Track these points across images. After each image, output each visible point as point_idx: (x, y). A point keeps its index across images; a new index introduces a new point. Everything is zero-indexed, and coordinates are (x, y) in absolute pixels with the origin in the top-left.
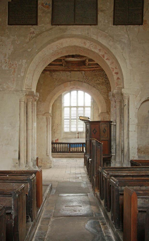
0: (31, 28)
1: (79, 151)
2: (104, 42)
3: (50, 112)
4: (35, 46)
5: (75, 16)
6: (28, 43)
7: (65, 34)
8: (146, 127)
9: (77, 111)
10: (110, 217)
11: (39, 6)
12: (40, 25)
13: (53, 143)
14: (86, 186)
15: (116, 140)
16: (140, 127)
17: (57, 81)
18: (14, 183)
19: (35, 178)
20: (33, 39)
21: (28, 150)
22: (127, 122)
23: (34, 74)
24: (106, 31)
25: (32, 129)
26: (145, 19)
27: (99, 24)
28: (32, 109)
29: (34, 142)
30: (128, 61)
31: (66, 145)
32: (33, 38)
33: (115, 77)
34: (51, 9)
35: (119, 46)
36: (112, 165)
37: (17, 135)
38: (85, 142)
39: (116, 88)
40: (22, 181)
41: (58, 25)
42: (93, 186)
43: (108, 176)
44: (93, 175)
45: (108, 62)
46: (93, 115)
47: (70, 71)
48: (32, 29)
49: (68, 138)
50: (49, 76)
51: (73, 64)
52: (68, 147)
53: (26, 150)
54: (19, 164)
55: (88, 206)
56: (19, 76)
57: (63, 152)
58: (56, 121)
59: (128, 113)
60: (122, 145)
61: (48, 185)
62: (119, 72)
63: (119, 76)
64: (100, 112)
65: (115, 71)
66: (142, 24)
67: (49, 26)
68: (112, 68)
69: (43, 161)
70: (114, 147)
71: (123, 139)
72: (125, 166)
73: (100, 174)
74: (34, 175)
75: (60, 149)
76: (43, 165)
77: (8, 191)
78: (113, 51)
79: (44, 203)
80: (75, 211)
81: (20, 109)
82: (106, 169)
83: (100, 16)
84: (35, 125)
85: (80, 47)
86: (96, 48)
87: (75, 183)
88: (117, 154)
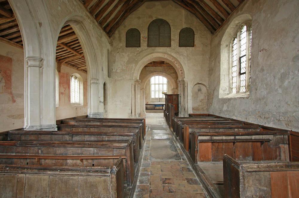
2: (174, 55)
6: (135, 56)
10: (178, 139)
11: (141, 38)
12: (142, 47)
15: (181, 104)
30: (186, 65)
33: (180, 72)
34: (147, 39)
35: (182, 57)
36: (179, 116)
37: (130, 101)
38: (165, 104)
40: (139, 123)
42: (169, 127)
43: (177, 121)
44: (169, 121)
45: (177, 65)
47: (156, 66)
48: (138, 49)
52: (154, 107)
55: (168, 135)
62: (182, 70)
63: (182, 72)
64: (172, 88)
66: (194, 47)
67: (146, 48)
72: (186, 116)
73: (173, 120)
74: (143, 120)
81: (132, 88)
83: (172, 43)
84: (139, 96)
85: (162, 58)
87: (160, 125)
88: (182, 111)
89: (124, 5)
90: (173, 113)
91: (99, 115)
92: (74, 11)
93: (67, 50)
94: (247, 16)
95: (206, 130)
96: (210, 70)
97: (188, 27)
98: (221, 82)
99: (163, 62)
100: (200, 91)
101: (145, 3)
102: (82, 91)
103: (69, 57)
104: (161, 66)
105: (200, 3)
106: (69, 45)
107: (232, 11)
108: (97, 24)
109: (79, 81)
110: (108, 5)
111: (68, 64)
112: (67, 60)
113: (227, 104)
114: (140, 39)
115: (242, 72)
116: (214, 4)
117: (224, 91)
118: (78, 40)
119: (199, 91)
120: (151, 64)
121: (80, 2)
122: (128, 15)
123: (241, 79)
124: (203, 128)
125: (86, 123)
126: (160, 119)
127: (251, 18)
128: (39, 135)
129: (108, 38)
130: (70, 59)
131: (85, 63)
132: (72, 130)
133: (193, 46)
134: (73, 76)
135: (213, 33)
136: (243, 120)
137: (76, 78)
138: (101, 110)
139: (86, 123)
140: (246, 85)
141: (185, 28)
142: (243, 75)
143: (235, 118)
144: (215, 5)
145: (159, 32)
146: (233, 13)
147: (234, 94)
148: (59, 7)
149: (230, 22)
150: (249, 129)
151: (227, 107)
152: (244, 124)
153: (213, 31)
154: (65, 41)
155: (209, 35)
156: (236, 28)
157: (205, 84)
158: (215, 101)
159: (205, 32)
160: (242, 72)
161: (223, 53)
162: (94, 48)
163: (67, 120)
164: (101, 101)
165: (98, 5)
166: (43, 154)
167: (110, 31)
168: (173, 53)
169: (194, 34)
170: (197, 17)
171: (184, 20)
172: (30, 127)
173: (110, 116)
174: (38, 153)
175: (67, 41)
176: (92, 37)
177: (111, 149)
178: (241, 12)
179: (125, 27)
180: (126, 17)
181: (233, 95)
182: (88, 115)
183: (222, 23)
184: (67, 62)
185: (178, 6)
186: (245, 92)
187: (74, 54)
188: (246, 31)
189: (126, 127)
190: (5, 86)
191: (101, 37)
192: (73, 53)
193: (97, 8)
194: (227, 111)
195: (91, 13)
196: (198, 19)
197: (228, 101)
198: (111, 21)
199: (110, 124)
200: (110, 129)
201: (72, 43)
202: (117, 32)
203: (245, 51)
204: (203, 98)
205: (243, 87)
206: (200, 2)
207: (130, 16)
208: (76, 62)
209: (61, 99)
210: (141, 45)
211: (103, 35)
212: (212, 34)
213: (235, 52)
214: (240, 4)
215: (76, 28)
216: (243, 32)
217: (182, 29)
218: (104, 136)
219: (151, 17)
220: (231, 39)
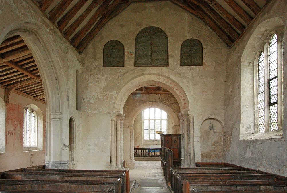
0: (119, 69)
1: (157, 155)
2: (174, 78)
3: (133, 125)
4: (122, 81)
5: (152, 60)
6: (117, 79)
7: (144, 72)
8: (208, 138)
9: (155, 123)
11: (126, 54)
12: (126, 67)
13: (135, 149)
14: (162, 182)
15: (184, 148)
16: (202, 138)
17: (138, 102)
18: (112, 178)
19: (126, 175)
20: (121, 77)
22: (192, 135)
24: (175, 70)
25: (120, 140)
27: (170, 65)
28: (120, 126)
29: (122, 149)
31: (146, 150)
32: (121, 76)
33: (183, 102)
34: (134, 55)
35: (185, 81)
36: (182, 167)
39: (184, 111)
40: (118, 177)
41: (140, 67)
42: (167, 182)
43: (176, 174)
45: (177, 92)
46: (169, 126)
47: (149, 94)
48: (120, 69)
49: (148, 145)
52: (148, 152)
53: (116, 156)
54: (111, 166)
56: (111, 102)
57: (143, 156)
58: (138, 131)
59: (193, 128)
60: (189, 152)
61: (133, 181)
63: (185, 101)
64: (173, 125)
65: (183, 98)
66: (202, 65)
67: (133, 67)
68: (180, 96)
69: (128, 163)
71: (189, 147)
72: (191, 167)
74: (124, 173)
75: (141, 153)
76: (127, 166)
77: (111, 182)
78: (181, 85)
82: (175, 169)
83: (171, 60)
84: (122, 137)
85: (156, 81)
86: (167, 82)
89: (99, 8)
90: (171, 160)
91: (61, 164)
92: (23, 16)
94: (275, 21)
95: (216, 187)
96: (226, 98)
97: (194, 38)
98: (242, 116)
99: (159, 88)
100: (212, 130)
101: (131, 5)
102: (41, 130)
103: (21, 81)
104: (156, 94)
105: (210, 4)
106: (20, 64)
107: (256, 15)
108: (59, 34)
109: (37, 115)
110: (77, 8)
111: (21, 91)
112: (19, 85)
113: (251, 148)
115: (272, 102)
117: (247, 129)
118: (32, 57)
119: (211, 129)
120: (142, 90)
121: (33, 4)
122: (107, 22)
123: (271, 112)
124: (211, 185)
125: (40, 178)
126: (156, 171)
127: (282, 23)
129: (77, 54)
130: (24, 84)
131: (43, 91)
132: (16, 187)
133: (201, 65)
134: (27, 108)
135: (230, 46)
136: (275, 172)
137: (32, 111)
138: (66, 158)
139: (40, 178)
140: (279, 120)
141: (189, 39)
142: (273, 106)
143: (262, 169)
144: (230, 6)
145: (151, 45)
146: (258, 16)
147: (261, 134)
149: (252, 30)
150: (283, 186)
152: (277, 178)
154: (14, 58)
155: (224, 49)
156: (262, 38)
157: (219, 119)
158: (233, 143)
159: (218, 45)
160: (272, 102)
161: (245, 74)
162: (55, 69)
163: (11, 173)
164: (66, 144)
165: (61, 8)
167: (80, 44)
168: (171, 74)
169: (202, 48)
170: (206, 23)
171: (187, 28)
173: (79, 167)
175: (17, 59)
176: (52, 54)
178: (268, 15)
179: (102, 38)
180: (104, 24)
181: (261, 134)
182: (46, 165)
183: (242, 31)
184: (20, 89)
186: (278, 131)
187: (28, 77)
188: (277, 42)
189: (97, 183)
191: (66, 53)
192: (27, 76)
194: (251, 158)
195: (52, 18)
196: (208, 27)
197: (253, 144)
198: (81, 30)
199: (75, 178)
200: (73, 185)
202: (90, 46)
203: (276, 70)
204: (217, 140)
205: (274, 123)
206: (210, 3)
207: (109, 23)
208: (33, 89)
209: (8, 142)
210: (125, 63)
213: (262, 73)
214: (266, 4)
215: (28, 40)
216: (273, 43)
217: (185, 41)
219: (139, 24)
220: (256, 55)
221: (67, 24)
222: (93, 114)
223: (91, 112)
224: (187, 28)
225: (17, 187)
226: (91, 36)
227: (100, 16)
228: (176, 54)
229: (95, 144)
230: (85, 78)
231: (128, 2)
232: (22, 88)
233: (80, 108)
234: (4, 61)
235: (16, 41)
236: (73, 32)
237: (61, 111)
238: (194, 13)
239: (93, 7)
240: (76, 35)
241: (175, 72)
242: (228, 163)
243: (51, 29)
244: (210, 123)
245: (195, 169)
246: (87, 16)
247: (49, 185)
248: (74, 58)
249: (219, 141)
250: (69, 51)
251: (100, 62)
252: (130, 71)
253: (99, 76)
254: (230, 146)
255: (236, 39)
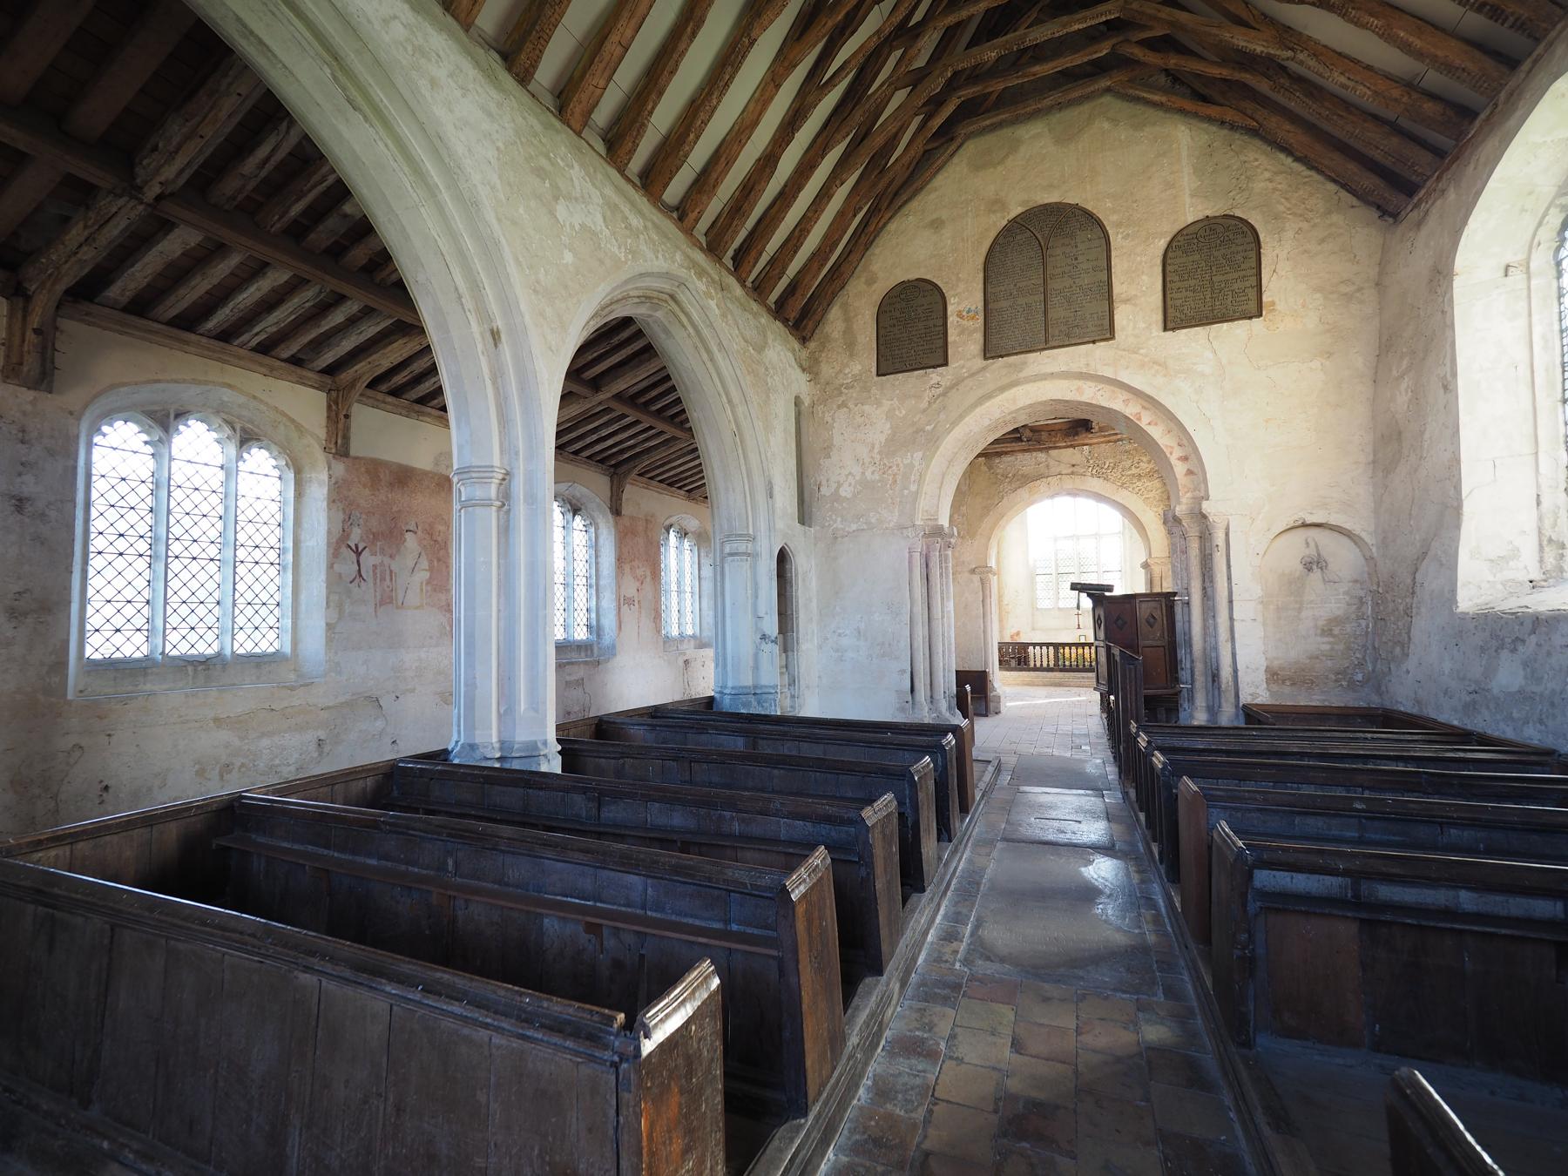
4: (942, 416)
6: (924, 411)
7: (1022, 375)
11: (952, 319)
12: (954, 364)
16: (1271, 607)
21: (934, 670)
23: (942, 483)
25: (943, 617)
26: (1270, 299)
28: (941, 568)
29: (950, 650)
41: (1002, 357)
48: (935, 376)
50: (984, 468)
51: (1053, 433)
56: (906, 492)
59: (1229, 567)
67: (980, 362)
68: (1167, 446)
70: (1188, 666)
74: (950, 736)
79: (979, 804)
80: (1063, 832)
83: (1121, 316)
92: (630, 257)
93: (637, 422)
102: (708, 586)
104: (1072, 446)
106: (643, 400)
108: (738, 290)
111: (651, 478)
112: (646, 462)
114: (945, 324)
116: (1387, 36)
128: (486, 786)
129: (796, 345)
131: (701, 475)
134: (671, 526)
148: (566, 252)
151: (1522, 673)
153: (1394, 198)
154: (625, 386)
164: (768, 632)
166: (461, 877)
167: (806, 313)
172: (463, 746)
174: (442, 868)
177: (716, 892)
179: (871, 281)
180: (877, 233)
185: (1151, 112)
190: (428, 583)
191: (760, 349)
192: (662, 433)
193: (735, 223)
195: (713, 247)
196: (1282, 156)
198: (805, 265)
201: (654, 393)
202: (835, 313)
206: (1290, 53)
207: (892, 226)
208: (682, 469)
211: (770, 337)
212: (1391, 220)
218: (727, 814)
219: (997, 204)
221: (761, 254)
222: (849, 533)
223: (843, 529)
224: (1186, 179)
225: (627, 766)
226: (837, 279)
227: (861, 209)
228: (1144, 288)
229: (859, 633)
230: (823, 418)
231: (952, 139)
232: (654, 469)
233: (810, 518)
234: (602, 396)
235: (625, 334)
236: (780, 278)
237: (751, 532)
238: (1213, 115)
239: (838, 182)
240: (789, 285)
241: (1141, 357)
242: (1402, 709)
243: (713, 281)
244: (1307, 544)
245: (1236, 732)
246: (818, 219)
247: (710, 765)
248: (785, 361)
249: (1353, 616)
250: (770, 341)
251: (867, 360)
252: (967, 377)
253: (866, 408)
254: (1409, 638)
255: (1429, 178)
